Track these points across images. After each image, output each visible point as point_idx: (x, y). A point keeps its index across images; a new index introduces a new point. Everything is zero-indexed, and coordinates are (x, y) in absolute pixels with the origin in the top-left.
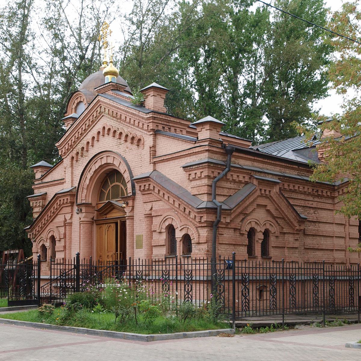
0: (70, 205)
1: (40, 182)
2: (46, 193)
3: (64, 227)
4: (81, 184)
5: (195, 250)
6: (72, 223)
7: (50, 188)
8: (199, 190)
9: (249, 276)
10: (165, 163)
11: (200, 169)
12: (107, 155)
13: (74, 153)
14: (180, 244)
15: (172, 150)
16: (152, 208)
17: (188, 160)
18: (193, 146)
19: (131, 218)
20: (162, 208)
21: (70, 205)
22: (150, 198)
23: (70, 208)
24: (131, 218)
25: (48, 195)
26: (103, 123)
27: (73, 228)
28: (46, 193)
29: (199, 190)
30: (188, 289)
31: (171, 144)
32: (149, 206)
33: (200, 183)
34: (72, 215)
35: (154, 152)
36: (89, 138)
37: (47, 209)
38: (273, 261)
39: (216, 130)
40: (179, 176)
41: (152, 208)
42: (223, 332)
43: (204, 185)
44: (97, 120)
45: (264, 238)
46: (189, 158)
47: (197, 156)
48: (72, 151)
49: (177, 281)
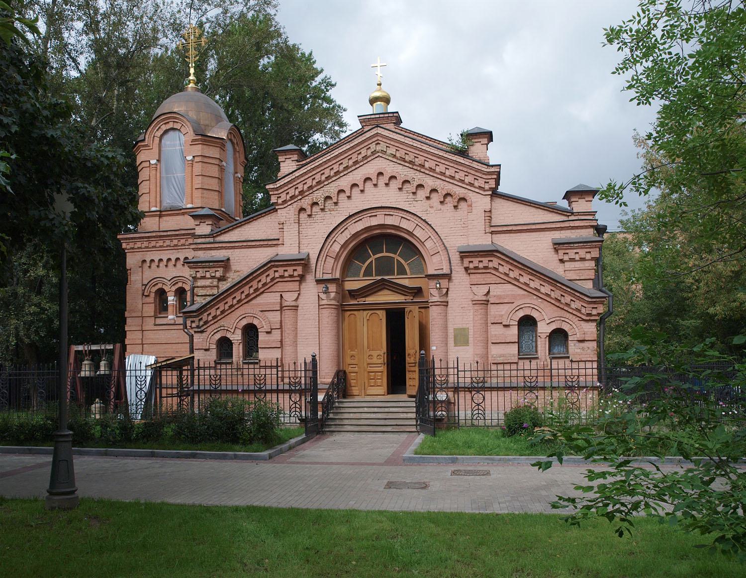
0: (298, 279)
1: (211, 240)
2: (228, 259)
3: (279, 312)
4: (324, 250)
5: (574, 348)
6: (298, 307)
7: (236, 250)
8: (580, 275)
9: (277, 374)
10: (512, 235)
11: (586, 248)
12: (403, 216)
13: (306, 203)
14: (545, 341)
15: (524, 220)
16: (489, 292)
17: (555, 236)
18: (565, 218)
19: (444, 304)
20: (510, 293)
21: (298, 279)
22: (486, 279)
23: (298, 283)
24: (444, 304)
25: (232, 261)
26: (376, 167)
27: (299, 313)
28: (228, 259)
29: (580, 275)
30: (141, 396)
31: (521, 212)
32: (484, 289)
33: (582, 265)
34: (299, 294)
35: (489, 218)
36: (344, 182)
37: (243, 283)
38: (572, 361)
39: (584, 200)
40: (539, 254)
41: (489, 292)
42: (210, 455)
43: (590, 268)
44: (365, 162)
45: (599, 336)
46: (559, 232)
47: (562, 232)
48: (301, 199)
49: (167, 388)
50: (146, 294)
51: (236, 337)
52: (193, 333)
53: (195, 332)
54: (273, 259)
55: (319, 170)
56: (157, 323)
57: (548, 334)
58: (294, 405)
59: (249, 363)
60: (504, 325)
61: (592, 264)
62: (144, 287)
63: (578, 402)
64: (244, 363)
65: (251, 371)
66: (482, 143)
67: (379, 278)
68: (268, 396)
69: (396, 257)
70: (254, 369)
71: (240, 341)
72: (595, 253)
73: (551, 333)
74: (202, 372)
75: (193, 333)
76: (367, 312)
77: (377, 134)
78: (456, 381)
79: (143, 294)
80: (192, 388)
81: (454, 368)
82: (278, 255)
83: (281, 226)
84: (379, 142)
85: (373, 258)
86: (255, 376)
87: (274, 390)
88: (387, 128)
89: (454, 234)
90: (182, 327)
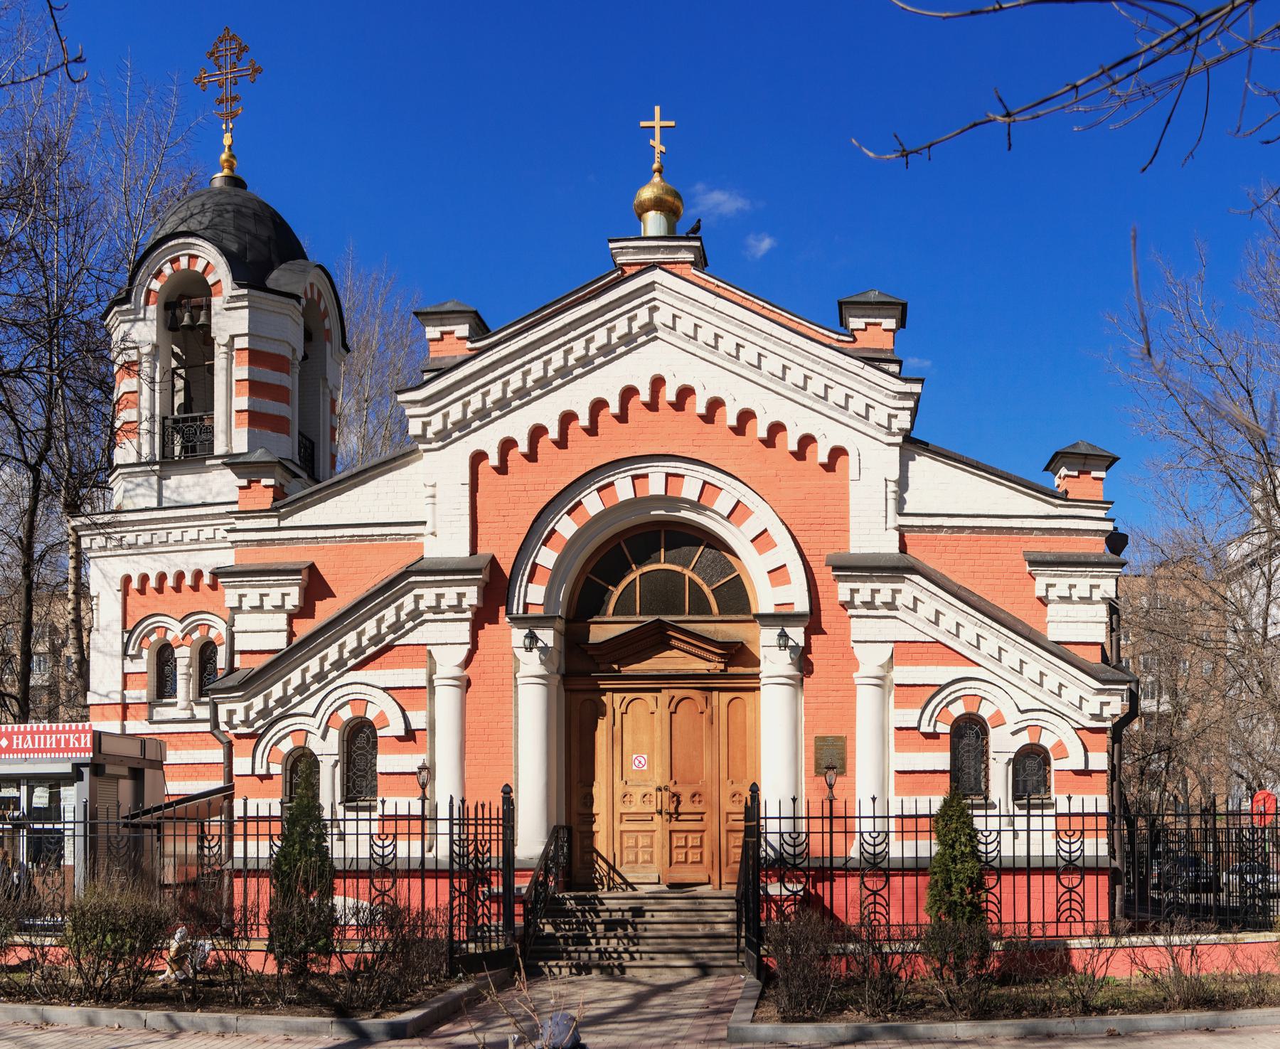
1: (273, 522)
50: (131, 652)
51: (327, 749)
52: (233, 738)
53: (238, 736)
54: (413, 568)
55: (518, 362)
56: (155, 718)
57: (1012, 756)
58: (1067, 896)
59: (357, 809)
60: (923, 734)
61: (1102, 611)
62: (126, 635)
63: (886, 890)
64: (347, 809)
65: (364, 827)
66: (884, 326)
67: (649, 619)
68: (403, 884)
69: (688, 573)
70: (357, 820)
71: (337, 758)
72: (1108, 587)
73: (1018, 753)
74: (252, 827)
75: (233, 738)
76: (623, 695)
77: (650, 287)
78: (827, 854)
79: (125, 654)
80: (229, 865)
81: (823, 818)
82: (422, 558)
83: (430, 491)
84: (656, 303)
85: (635, 575)
86: (371, 837)
87: (416, 871)
88: (679, 273)
89: (818, 527)
90: (207, 727)
